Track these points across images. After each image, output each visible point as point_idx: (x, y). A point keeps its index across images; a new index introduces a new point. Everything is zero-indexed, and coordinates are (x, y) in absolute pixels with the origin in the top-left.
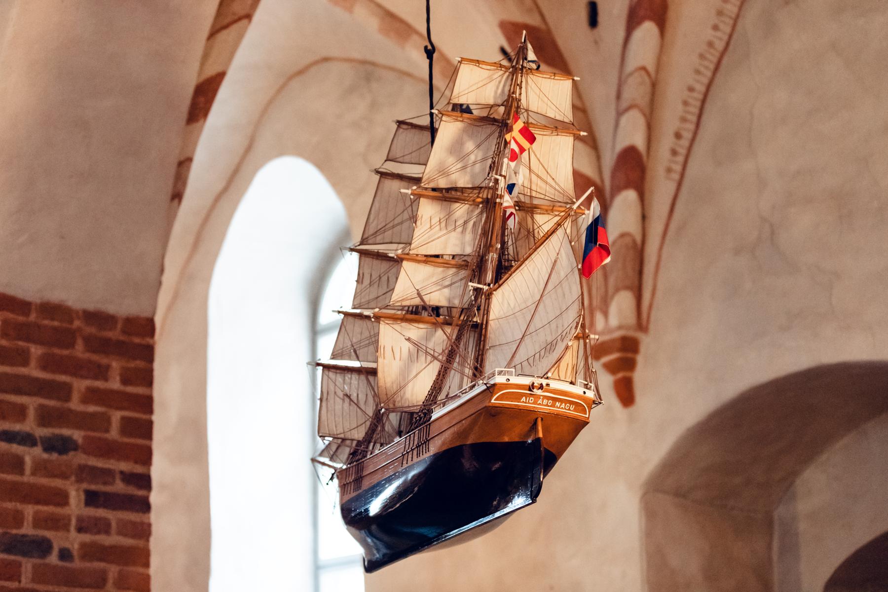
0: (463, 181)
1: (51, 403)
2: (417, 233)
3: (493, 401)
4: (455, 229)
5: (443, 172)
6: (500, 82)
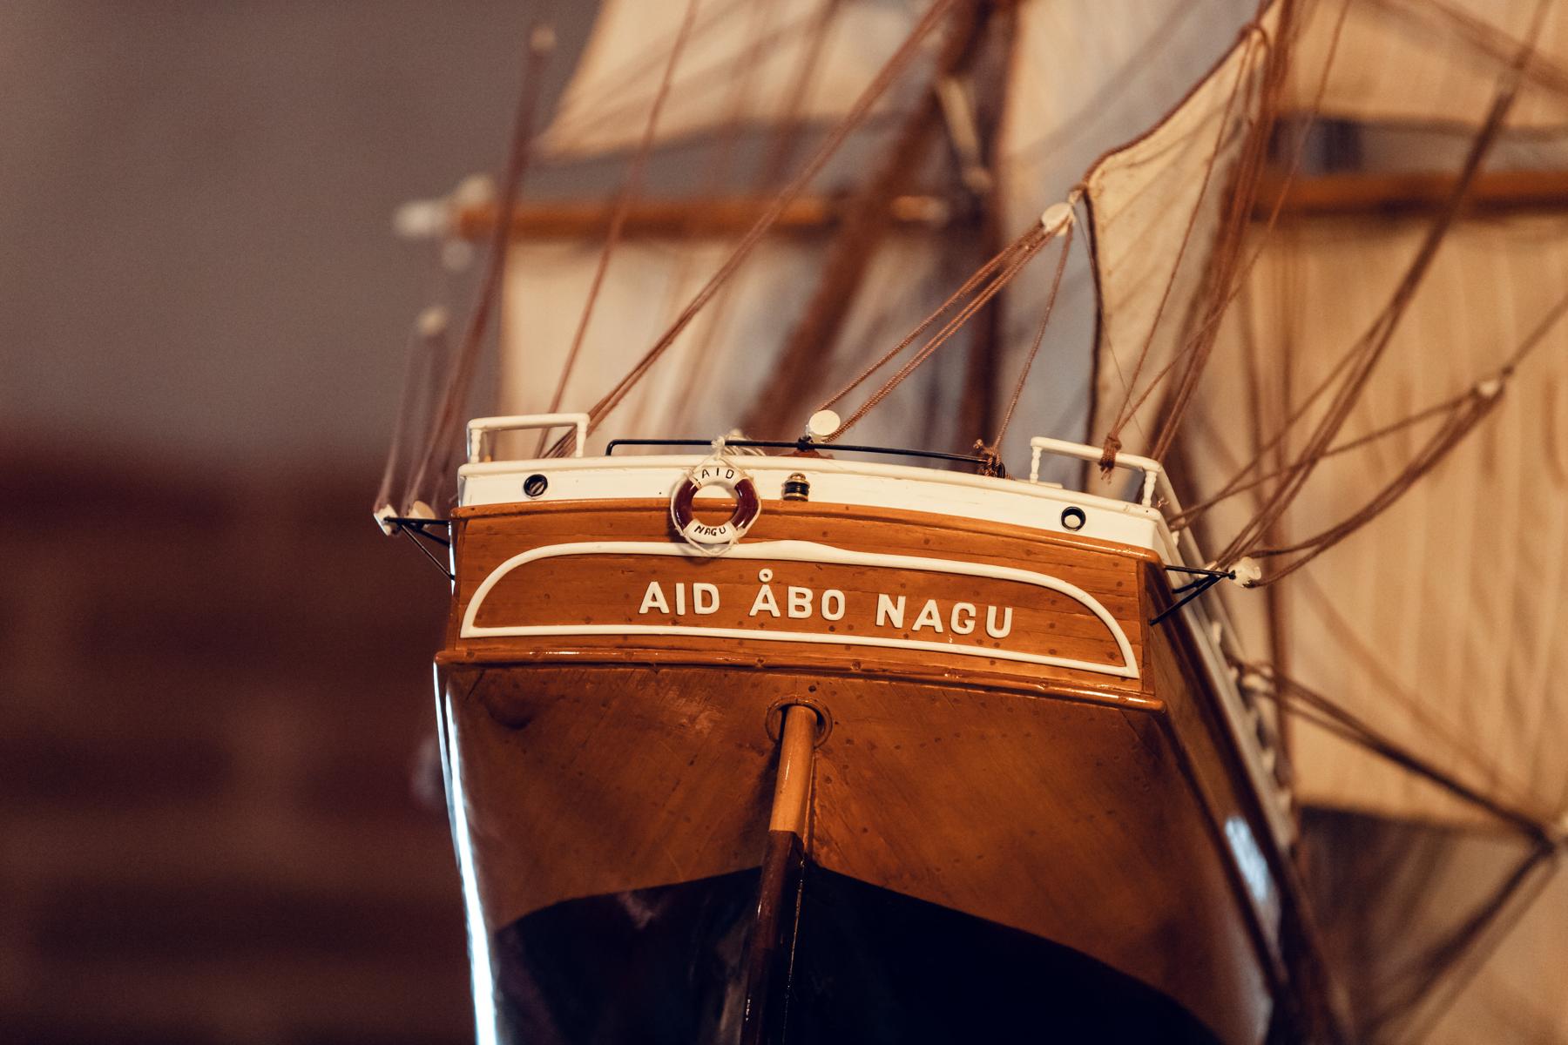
3: (469, 630)
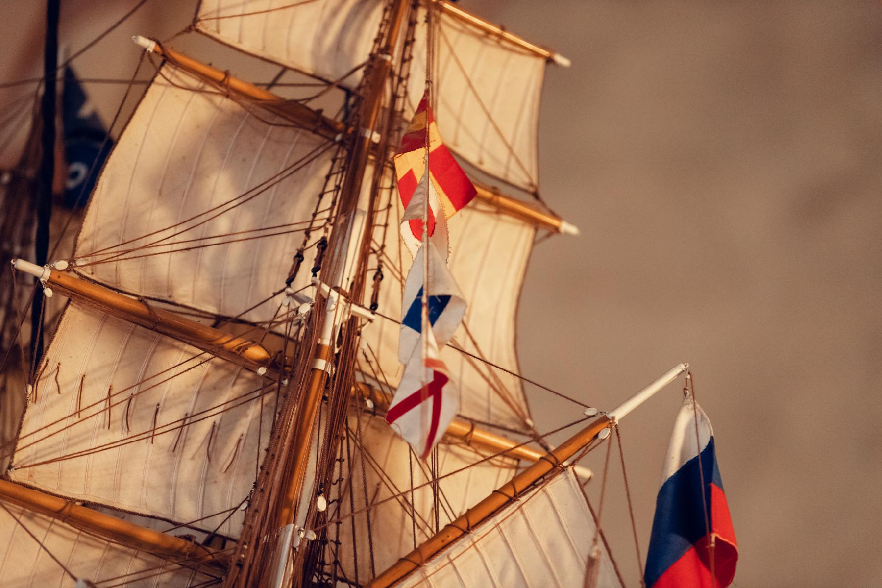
0: (192, 290)
1: (99, 154)
2: (33, 421)
4: (152, 435)
5: (131, 246)
6: (335, 13)
